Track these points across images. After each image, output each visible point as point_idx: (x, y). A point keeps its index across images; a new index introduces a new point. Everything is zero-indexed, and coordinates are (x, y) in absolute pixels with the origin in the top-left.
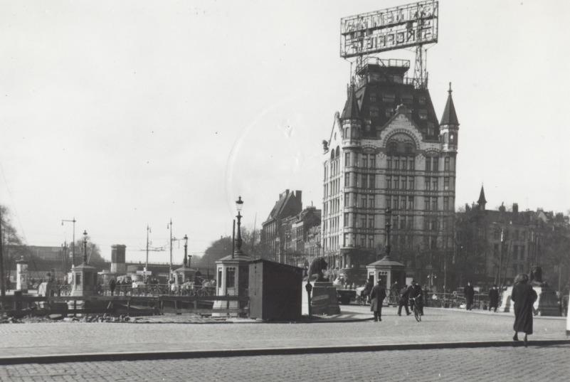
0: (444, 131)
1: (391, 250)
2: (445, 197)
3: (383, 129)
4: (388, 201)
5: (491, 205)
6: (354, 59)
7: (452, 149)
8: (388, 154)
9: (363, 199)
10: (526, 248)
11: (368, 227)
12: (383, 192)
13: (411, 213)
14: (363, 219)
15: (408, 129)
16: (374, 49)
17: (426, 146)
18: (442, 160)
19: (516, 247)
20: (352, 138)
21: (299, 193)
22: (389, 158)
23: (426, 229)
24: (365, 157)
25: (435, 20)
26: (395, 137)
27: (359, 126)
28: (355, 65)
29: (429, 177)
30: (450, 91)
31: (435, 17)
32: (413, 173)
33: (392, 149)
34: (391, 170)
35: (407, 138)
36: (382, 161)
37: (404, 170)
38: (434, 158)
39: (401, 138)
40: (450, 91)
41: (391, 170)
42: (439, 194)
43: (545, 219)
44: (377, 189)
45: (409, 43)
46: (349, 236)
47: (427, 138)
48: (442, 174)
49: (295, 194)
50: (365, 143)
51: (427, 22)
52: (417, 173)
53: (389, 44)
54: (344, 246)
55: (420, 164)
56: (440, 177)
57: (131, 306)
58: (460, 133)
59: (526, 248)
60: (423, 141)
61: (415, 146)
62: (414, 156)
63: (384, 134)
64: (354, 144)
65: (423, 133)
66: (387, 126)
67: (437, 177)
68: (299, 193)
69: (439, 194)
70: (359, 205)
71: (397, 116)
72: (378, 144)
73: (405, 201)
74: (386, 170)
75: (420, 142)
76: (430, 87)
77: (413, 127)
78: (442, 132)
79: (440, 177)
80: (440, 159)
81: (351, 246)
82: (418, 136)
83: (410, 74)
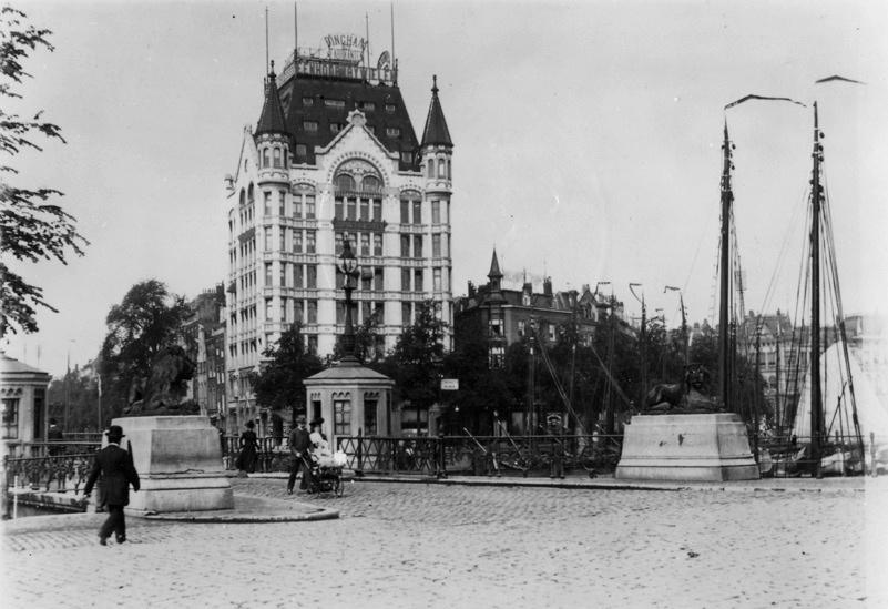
75: (389, 174)
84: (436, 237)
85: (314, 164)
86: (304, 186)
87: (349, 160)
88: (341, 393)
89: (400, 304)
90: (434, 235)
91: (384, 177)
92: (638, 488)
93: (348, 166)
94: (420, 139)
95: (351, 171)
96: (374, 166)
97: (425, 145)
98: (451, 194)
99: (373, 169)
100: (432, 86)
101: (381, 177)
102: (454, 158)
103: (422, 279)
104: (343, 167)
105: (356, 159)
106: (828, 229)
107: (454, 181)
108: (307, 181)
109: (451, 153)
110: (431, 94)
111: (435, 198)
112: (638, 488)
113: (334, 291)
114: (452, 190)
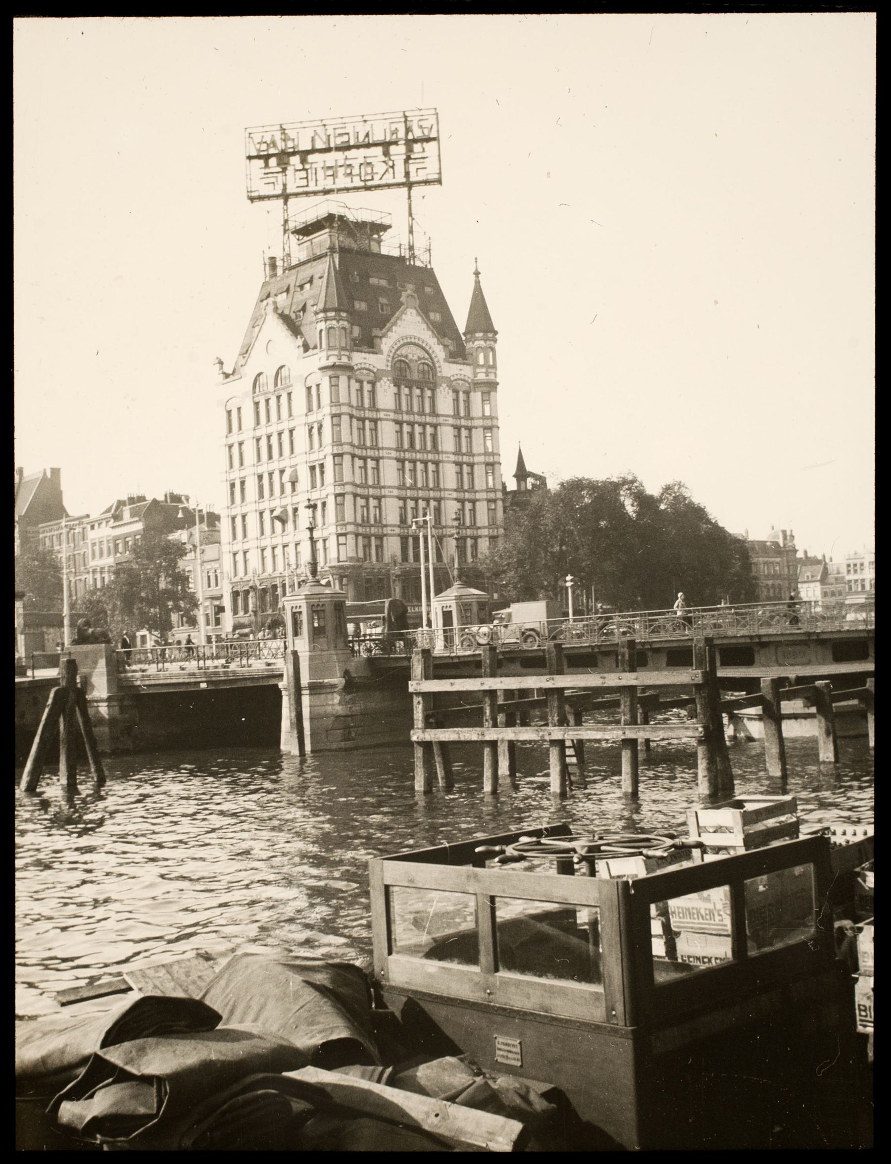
1: (319, 569)
11: (372, 522)
13: (377, 492)
14: (93, 527)
15: (422, 337)
17: (449, 370)
18: (476, 397)
20: (330, 348)
21: (56, 472)
25: (433, 144)
31: (434, 139)
35: (422, 354)
38: (464, 392)
43: (630, 508)
44: (383, 448)
45: (383, 182)
49: (49, 475)
51: (417, 147)
53: (343, 181)
55: (445, 403)
56: (476, 428)
57: (416, 700)
60: (445, 360)
63: (387, 344)
66: (390, 330)
67: (469, 429)
68: (56, 472)
72: (378, 362)
73: (414, 471)
75: (441, 361)
77: (430, 333)
79: (476, 428)
80: (472, 394)
82: (439, 353)
84: (339, 499)
85: (373, 347)
86: (365, 372)
87: (405, 344)
88: (318, 605)
89: (398, 539)
90: (337, 495)
91: (437, 365)
92: (262, 523)
93: (404, 351)
94: (461, 327)
95: (406, 357)
96: (429, 354)
97: (469, 331)
98: (498, 384)
99: (427, 356)
100: (474, 270)
101: (433, 363)
102: (497, 346)
103: (401, 516)
104: (399, 352)
105: (414, 344)
106: (295, 521)
107: (235, 360)
108: (367, 366)
109: (495, 341)
110: (473, 277)
111: (485, 389)
112: (262, 523)
113: (399, 526)
114: (498, 380)
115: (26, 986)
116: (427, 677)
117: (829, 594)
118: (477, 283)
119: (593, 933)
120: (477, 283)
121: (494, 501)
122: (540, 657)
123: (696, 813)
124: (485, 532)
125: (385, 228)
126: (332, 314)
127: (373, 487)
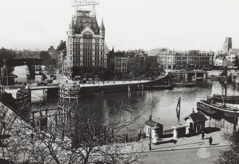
0: (101, 31)
2: (101, 51)
3: (82, 31)
4: (84, 46)
5: (115, 51)
6: (75, 7)
7: (103, 37)
8: (84, 38)
9: (76, 40)
10: (127, 64)
12: (83, 50)
16: (81, 5)
17: (95, 36)
19: (123, 69)
20: (72, 34)
22: (84, 39)
23: (96, 49)
24: (77, 39)
26: (86, 33)
27: (75, 30)
28: (75, 9)
29: (97, 45)
30: (102, 20)
32: (91, 44)
33: (85, 37)
34: (85, 43)
36: (82, 41)
37: (89, 49)
39: (88, 34)
40: (102, 20)
41: (85, 43)
42: (100, 50)
46: (72, 64)
47: (95, 33)
48: (100, 56)
50: (76, 35)
52: (93, 44)
53: (85, 4)
54: (71, 66)
58: (105, 32)
59: (127, 64)
61: (92, 36)
62: (92, 39)
63: (82, 33)
64: (73, 36)
65: (94, 32)
66: (83, 30)
67: (99, 45)
69: (100, 50)
70: (75, 42)
71: (86, 27)
74: (83, 43)
76: (97, 18)
78: (100, 32)
81: (73, 66)
82: (93, 33)
83: (91, 14)
93: (86, 33)
115: (149, 143)
116: (197, 77)
117: (172, 67)
118: (102, 21)
119: (52, 83)
120: (102, 21)
121: (102, 51)
122: (73, 69)
123: (180, 98)
124: (100, 56)
125: (90, 12)
126: (73, 29)
127: (90, 49)
